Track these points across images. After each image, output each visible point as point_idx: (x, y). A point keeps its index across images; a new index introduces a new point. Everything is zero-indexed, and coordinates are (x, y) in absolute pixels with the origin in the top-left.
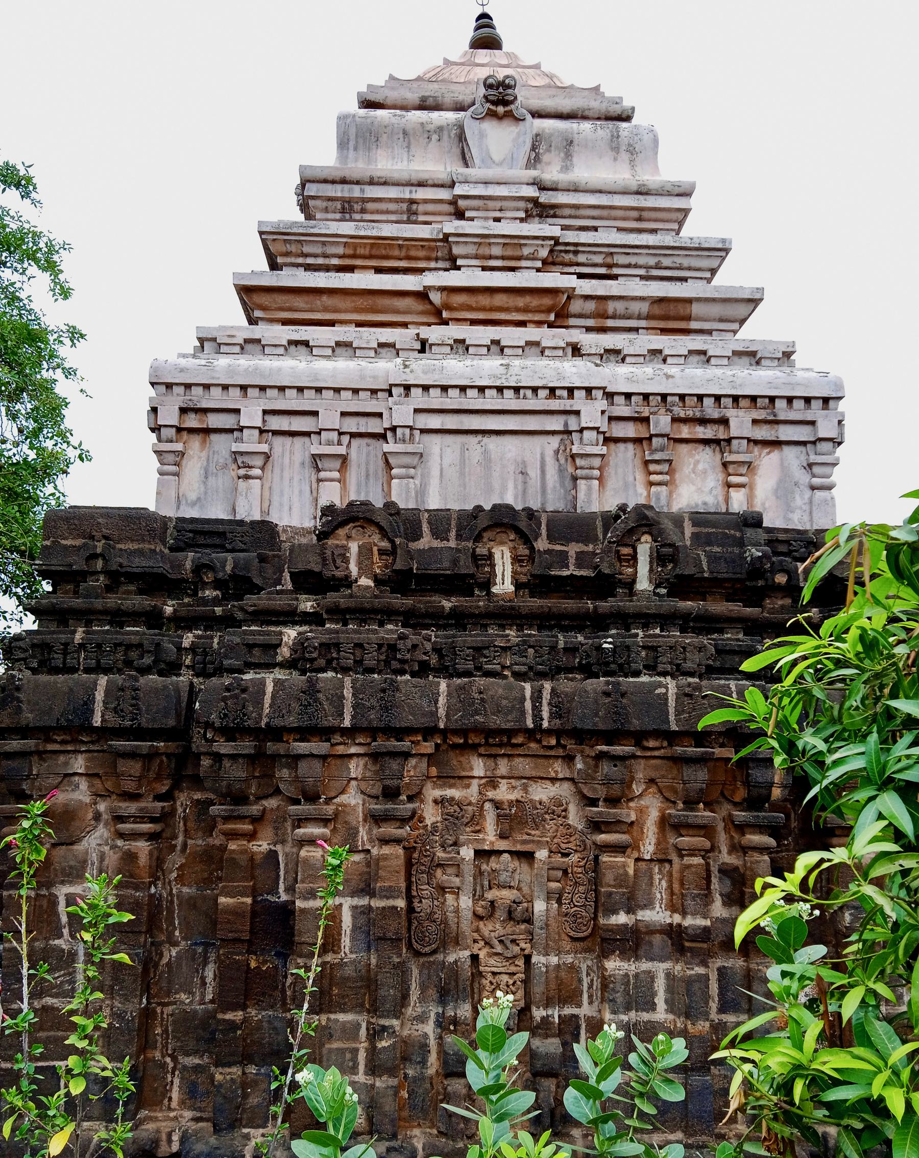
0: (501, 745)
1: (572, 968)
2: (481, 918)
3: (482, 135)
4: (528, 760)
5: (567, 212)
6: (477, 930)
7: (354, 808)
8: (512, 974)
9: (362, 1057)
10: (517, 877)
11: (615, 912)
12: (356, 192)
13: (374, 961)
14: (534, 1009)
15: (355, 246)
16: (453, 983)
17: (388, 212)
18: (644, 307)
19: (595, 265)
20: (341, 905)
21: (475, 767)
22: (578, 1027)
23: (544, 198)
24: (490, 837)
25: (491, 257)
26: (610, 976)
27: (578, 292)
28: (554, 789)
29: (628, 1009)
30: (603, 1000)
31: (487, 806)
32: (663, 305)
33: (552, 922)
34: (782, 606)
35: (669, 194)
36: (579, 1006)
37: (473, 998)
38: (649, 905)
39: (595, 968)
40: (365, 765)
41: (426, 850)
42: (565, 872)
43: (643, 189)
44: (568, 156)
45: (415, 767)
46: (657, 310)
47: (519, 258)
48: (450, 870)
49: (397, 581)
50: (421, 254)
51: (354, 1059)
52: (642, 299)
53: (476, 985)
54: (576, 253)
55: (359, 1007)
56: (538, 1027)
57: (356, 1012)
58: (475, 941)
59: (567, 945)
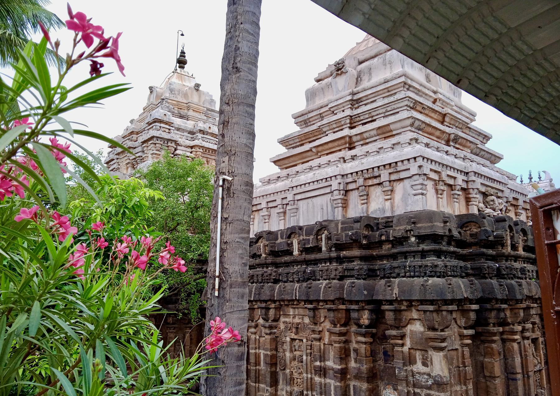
3: (336, 83)
5: (364, 99)
12: (306, 117)
15: (301, 138)
17: (316, 120)
18: (375, 132)
19: (367, 118)
23: (356, 97)
25: (334, 128)
27: (352, 134)
32: (381, 129)
34: (388, 248)
35: (396, 78)
38: (329, 360)
43: (386, 81)
44: (370, 74)
46: (379, 132)
47: (342, 125)
49: (273, 253)
50: (317, 133)
52: (373, 129)
54: (359, 117)
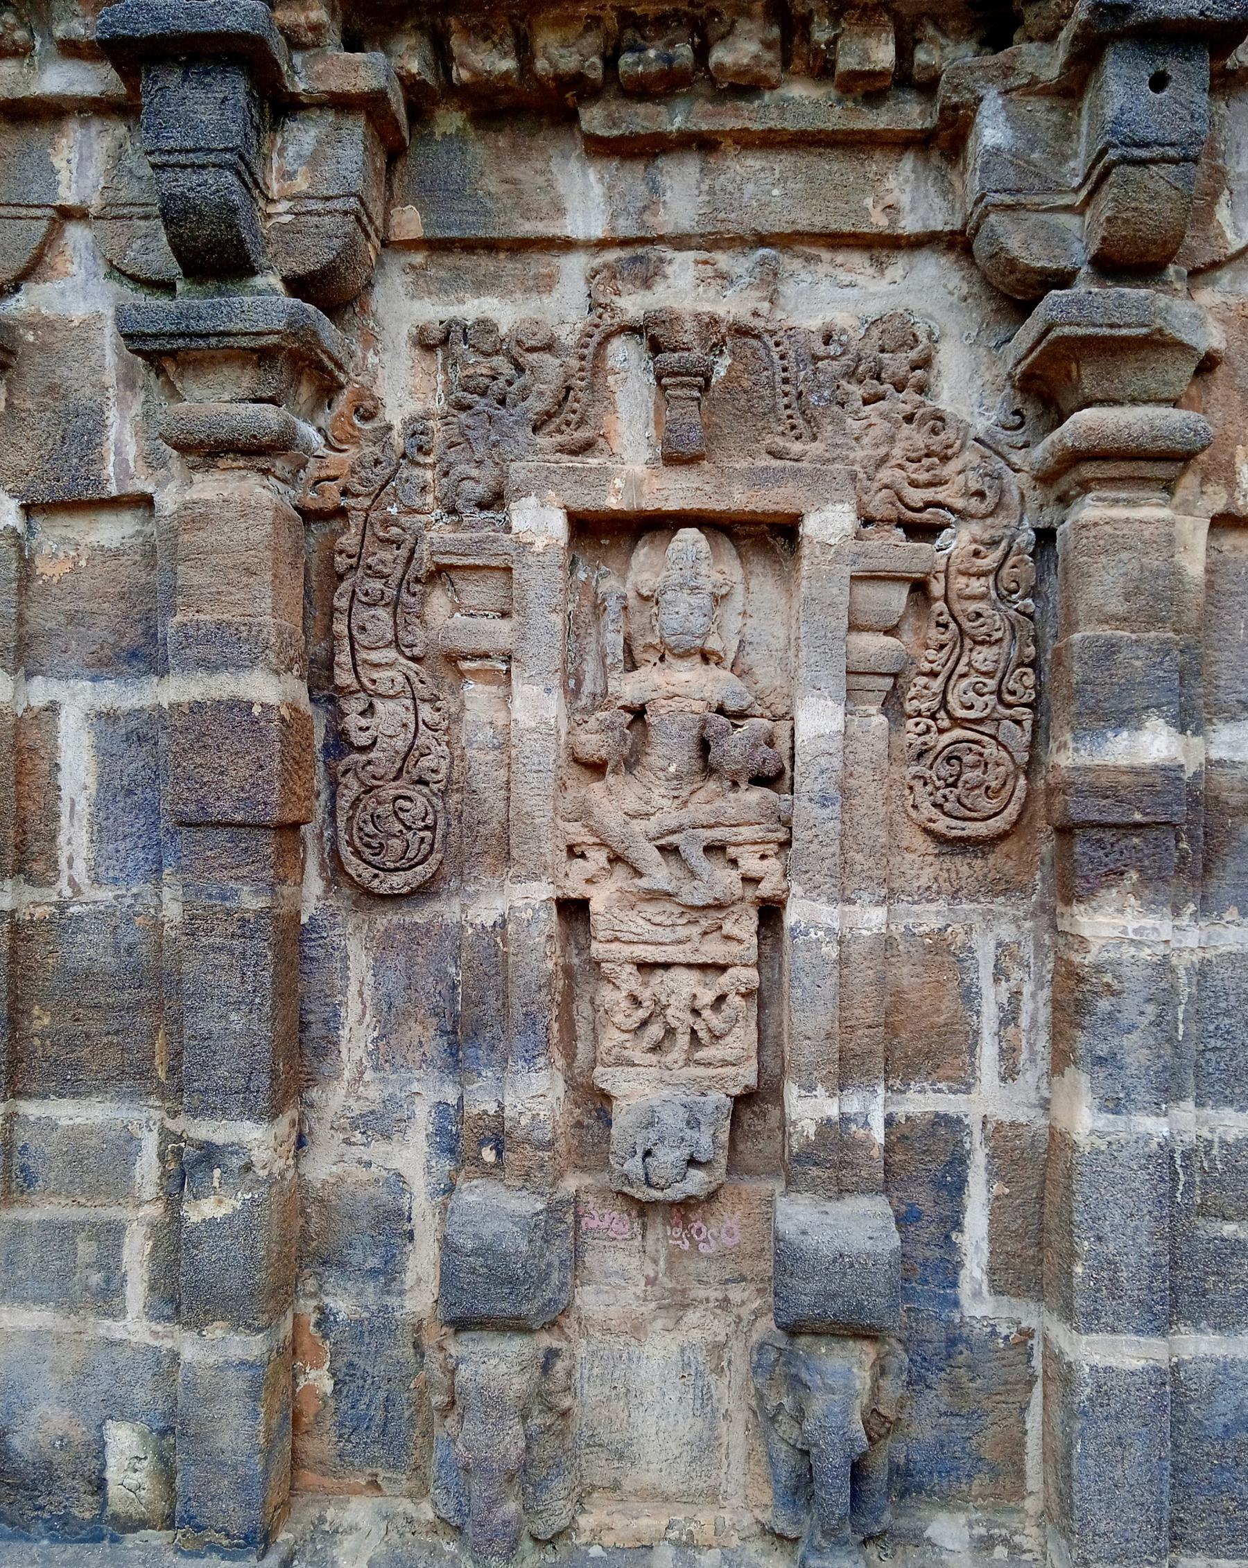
0: (665, 86)
1: (942, 952)
2: (596, 768)
4: (783, 163)
6: (584, 814)
7: (83, 333)
9: (136, 1254)
10: (733, 622)
11: (1126, 719)
13: (173, 911)
14: (791, 1091)
16: (493, 1002)
20: (53, 708)
21: (572, 202)
22: (959, 1161)
24: (631, 474)
26: (1099, 969)
28: (882, 285)
29: (1167, 1091)
30: (1061, 1060)
31: (623, 352)
33: (864, 780)
37: (570, 1056)
39: (1028, 952)
40: (117, 157)
41: (387, 523)
42: (919, 588)
45: (313, 161)
48: (477, 592)
51: (110, 1264)
53: (583, 1008)
55: (132, 1078)
56: (806, 1157)
57: (120, 1096)
59: (920, 864)
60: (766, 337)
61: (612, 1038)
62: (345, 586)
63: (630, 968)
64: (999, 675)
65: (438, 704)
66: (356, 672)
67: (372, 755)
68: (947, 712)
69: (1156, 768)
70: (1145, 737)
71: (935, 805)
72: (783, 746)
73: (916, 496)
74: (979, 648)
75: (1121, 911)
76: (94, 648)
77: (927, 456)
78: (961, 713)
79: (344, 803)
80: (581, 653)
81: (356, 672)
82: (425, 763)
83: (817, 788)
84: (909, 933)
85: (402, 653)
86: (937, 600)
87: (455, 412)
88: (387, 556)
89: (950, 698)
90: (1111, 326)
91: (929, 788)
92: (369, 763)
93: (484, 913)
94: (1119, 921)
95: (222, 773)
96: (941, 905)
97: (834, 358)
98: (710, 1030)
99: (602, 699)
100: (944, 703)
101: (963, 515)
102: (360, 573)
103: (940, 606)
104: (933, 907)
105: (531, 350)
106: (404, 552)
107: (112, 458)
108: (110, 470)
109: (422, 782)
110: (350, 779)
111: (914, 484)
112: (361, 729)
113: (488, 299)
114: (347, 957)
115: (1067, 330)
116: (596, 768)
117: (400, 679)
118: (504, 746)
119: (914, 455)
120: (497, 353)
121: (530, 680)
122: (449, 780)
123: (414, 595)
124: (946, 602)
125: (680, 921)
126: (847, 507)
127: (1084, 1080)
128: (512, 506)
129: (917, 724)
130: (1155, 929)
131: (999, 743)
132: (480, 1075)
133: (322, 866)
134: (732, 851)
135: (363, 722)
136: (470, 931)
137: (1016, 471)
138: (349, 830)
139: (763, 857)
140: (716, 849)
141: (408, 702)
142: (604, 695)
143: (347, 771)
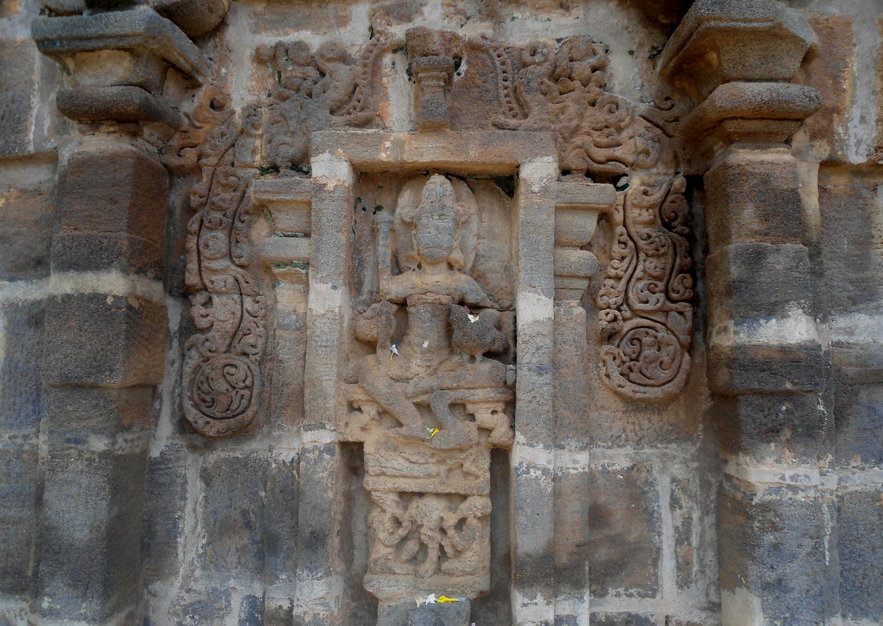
8: (457, 498)
11: (774, 310)
24: (397, 138)
36: (652, 590)
37: (349, 561)
58: (354, 408)
59: (610, 416)
60: (491, 51)
61: (380, 551)
62: (197, 216)
63: (393, 497)
64: (666, 278)
65: (258, 298)
66: (200, 275)
67: (210, 335)
68: (628, 305)
69: (800, 347)
70: (789, 323)
71: (622, 374)
72: (508, 328)
73: (601, 154)
74: (651, 259)
75: (778, 461)
76: (13, 258)
77: (607, 127)
78: (639, 306)
79: (188, 369)
80: (361, 263)
81: (200, 275)
82: (250, 339)
83: (534, 360)
84: (605, 471)
85: (233, 262)
86: (618, 225)
87: (278, 101)
88: (227, 196)
89: (630, 294)
90: (745, 21)
91: (618, 361)
92: (207, 340)
93: (285, 453)
94: (778, 469)
95: (81, 347)
96: (629, 450)
97: (539, 64)
98: (453, 546)
99: (376, 296)
100: (626, 299)
101: (633, 166)
102: (207, 208)
103: (620, 229)
104: (623, 451)
105: (329, 60)
106: (238, 194)
107: (33, 128)
108: (31, 136)
109: (245, 354)
110: (193, 353)
111: (598, 146)
112: (202, 316)
113: (304, 32)
114: (186, 482)
115: (712, 23)
116: (371, 346)
117: (231, 280)
118: (303, 328)
119: (598, 126)
120: (309, 65)
121: (323, 281)
122: (264, 353)
123: (243, 222)
124: (625, 225)
125: (431, 460)
126: (550, 159)
127: (756, 602)
128: (312, 159)
129: (607, 314)
130: (807, 476)
131: (668, 329)
132: (277, 578)
133: (173, 413)
134: (470, 408)
135: (203, 311)
136: (274, 466)
137: (671, 137)
138: (190, 389)
139: (494, 412)
140: (457, 406)
141: (236, 297)
142: (378, 292)
143: (192, 346)
